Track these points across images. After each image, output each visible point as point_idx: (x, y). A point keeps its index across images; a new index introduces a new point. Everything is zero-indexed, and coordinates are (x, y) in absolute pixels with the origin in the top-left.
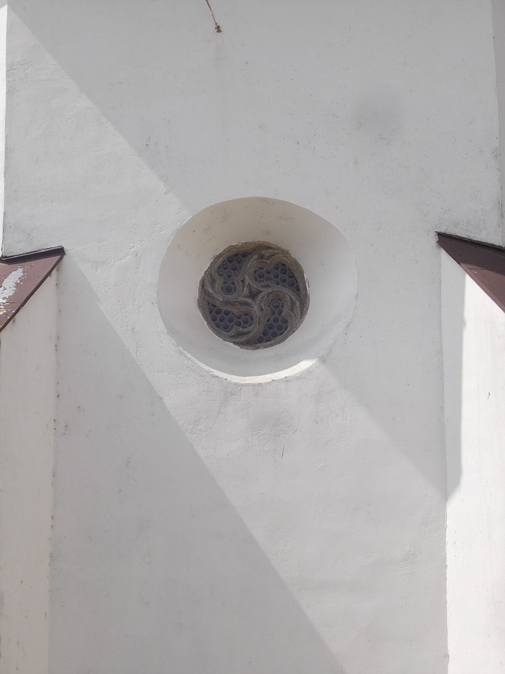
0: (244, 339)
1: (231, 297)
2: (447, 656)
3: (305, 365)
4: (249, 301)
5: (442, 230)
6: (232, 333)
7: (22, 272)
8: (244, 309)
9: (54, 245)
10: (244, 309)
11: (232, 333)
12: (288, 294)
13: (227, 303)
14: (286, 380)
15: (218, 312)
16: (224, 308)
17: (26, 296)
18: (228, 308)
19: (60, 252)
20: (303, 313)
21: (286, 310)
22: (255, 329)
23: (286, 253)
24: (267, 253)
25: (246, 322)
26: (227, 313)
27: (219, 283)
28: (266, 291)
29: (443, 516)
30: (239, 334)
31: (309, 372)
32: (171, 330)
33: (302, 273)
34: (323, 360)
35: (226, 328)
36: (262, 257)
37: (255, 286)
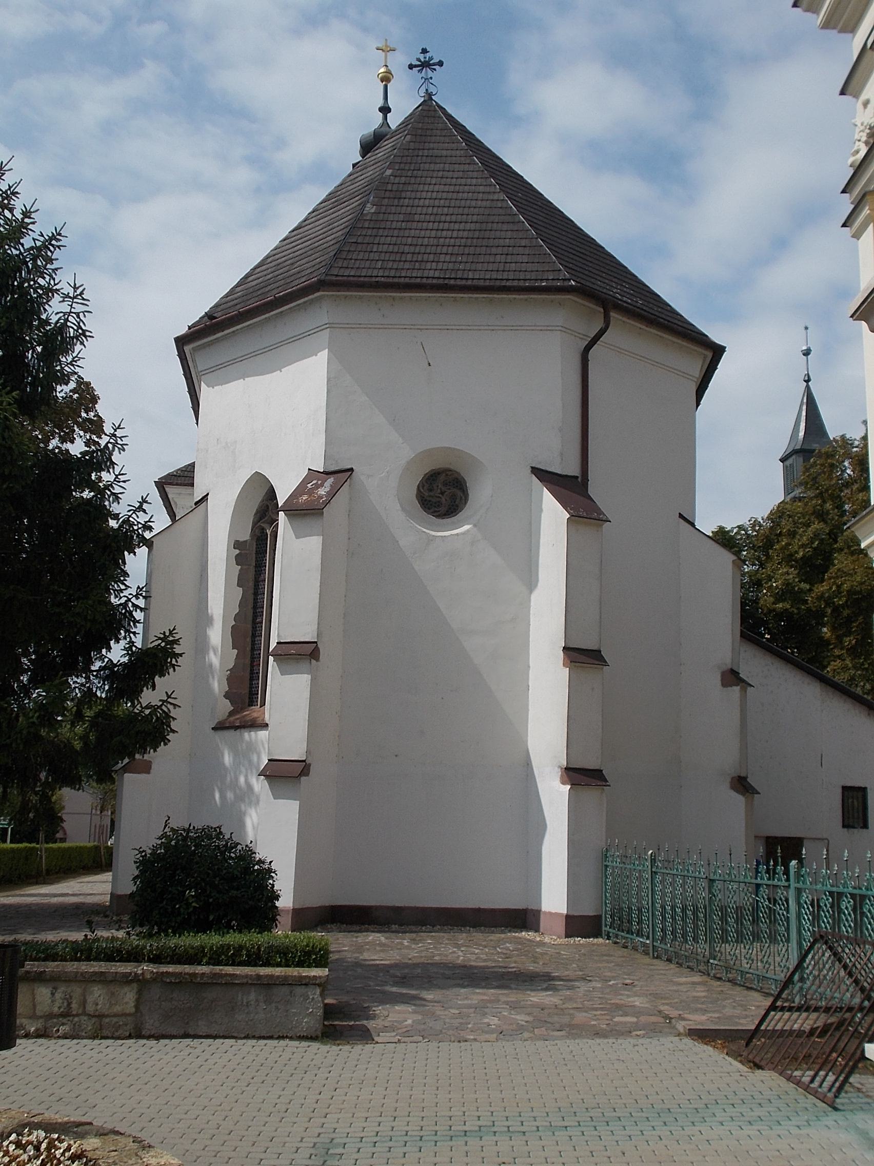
0: (437, 514)
1: (431, 494)
2: (529, 667)
3: (467, 527)
4: (440, 496)
5: (533, 466)
6: (431, 511)
7: (135, 554)
8: (438, 499)
9: (349, 467)
10: (438, 499)
11: (431, 511)
12: (459, 493)
13: (430, 496)
14: (457, 535)
15: (426, 500)
16: (428, 499)
17: (867, 35)
18: (430, 499)
19: (351, 470)
20: (466, 503)
21: (458, 500)
22: (443, 509)
23: (459, 474)
24: (449, 473)
25: (438, 506)
26: (430, 501)
27: (426, 486)
28: (449, 491)
29: (530, 601)
30: (435, 512)
31: (468, 531)
32: (403, 509)
33: (465, 483)
34: (475, 526)
35: (429, 509)
36: (447, 475)
37: (444, 489)
